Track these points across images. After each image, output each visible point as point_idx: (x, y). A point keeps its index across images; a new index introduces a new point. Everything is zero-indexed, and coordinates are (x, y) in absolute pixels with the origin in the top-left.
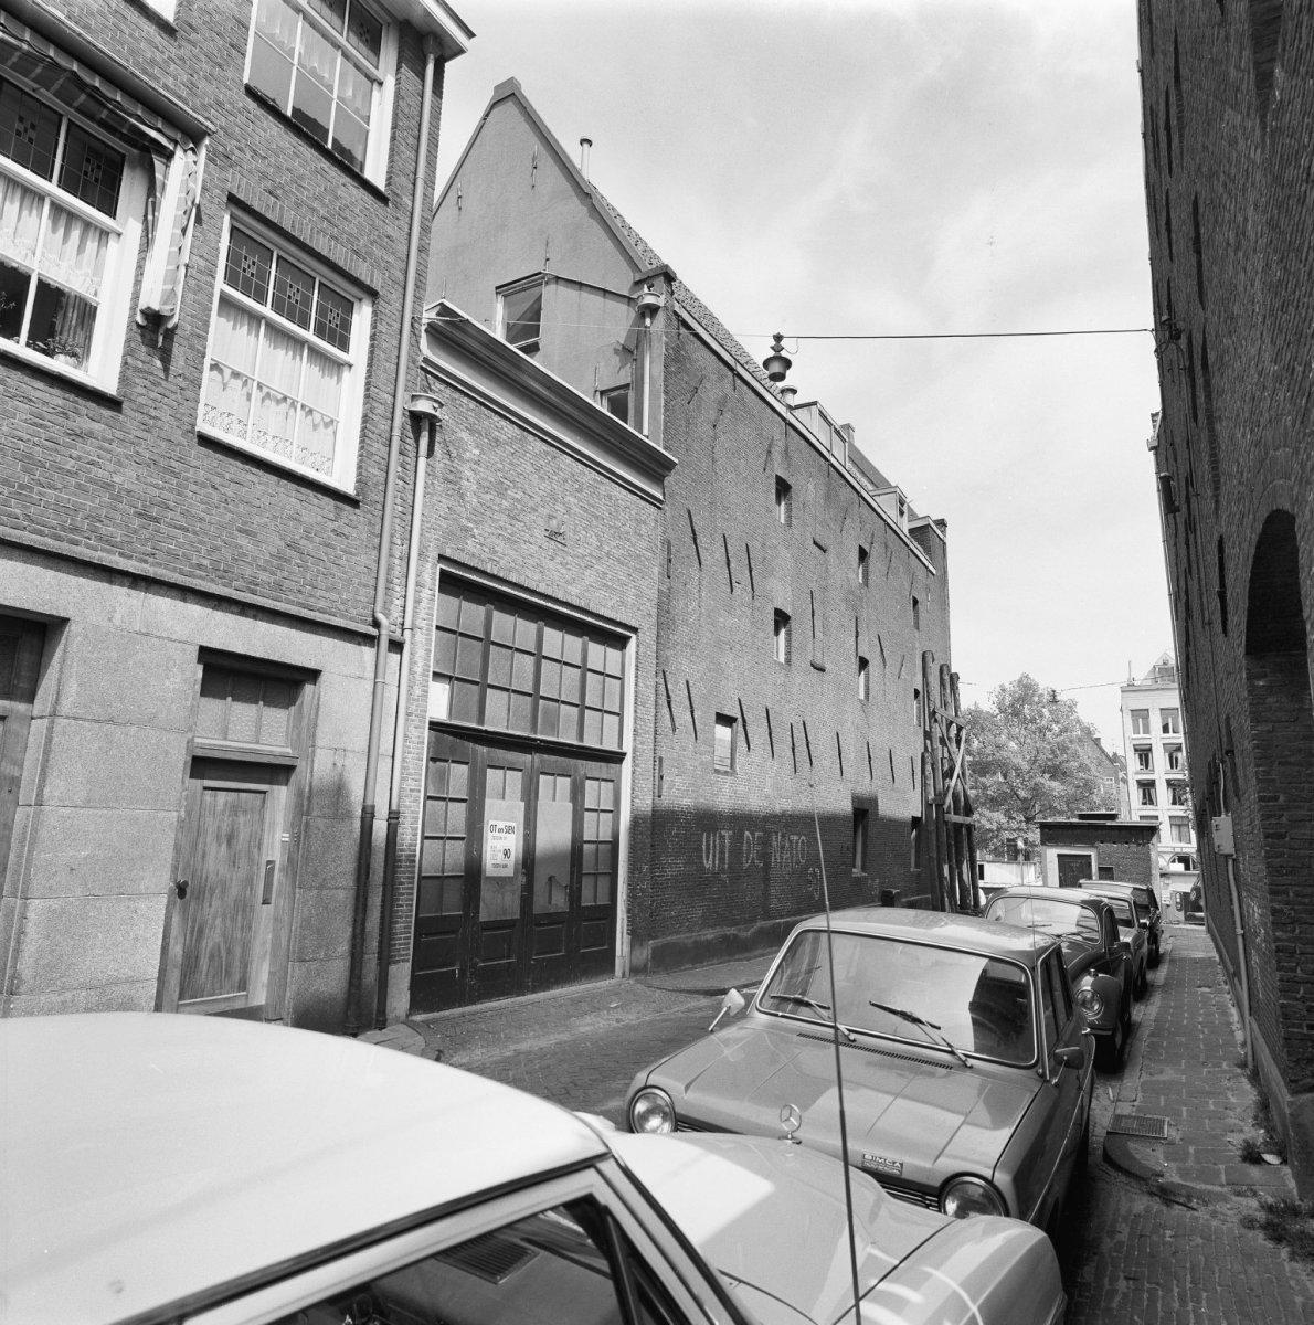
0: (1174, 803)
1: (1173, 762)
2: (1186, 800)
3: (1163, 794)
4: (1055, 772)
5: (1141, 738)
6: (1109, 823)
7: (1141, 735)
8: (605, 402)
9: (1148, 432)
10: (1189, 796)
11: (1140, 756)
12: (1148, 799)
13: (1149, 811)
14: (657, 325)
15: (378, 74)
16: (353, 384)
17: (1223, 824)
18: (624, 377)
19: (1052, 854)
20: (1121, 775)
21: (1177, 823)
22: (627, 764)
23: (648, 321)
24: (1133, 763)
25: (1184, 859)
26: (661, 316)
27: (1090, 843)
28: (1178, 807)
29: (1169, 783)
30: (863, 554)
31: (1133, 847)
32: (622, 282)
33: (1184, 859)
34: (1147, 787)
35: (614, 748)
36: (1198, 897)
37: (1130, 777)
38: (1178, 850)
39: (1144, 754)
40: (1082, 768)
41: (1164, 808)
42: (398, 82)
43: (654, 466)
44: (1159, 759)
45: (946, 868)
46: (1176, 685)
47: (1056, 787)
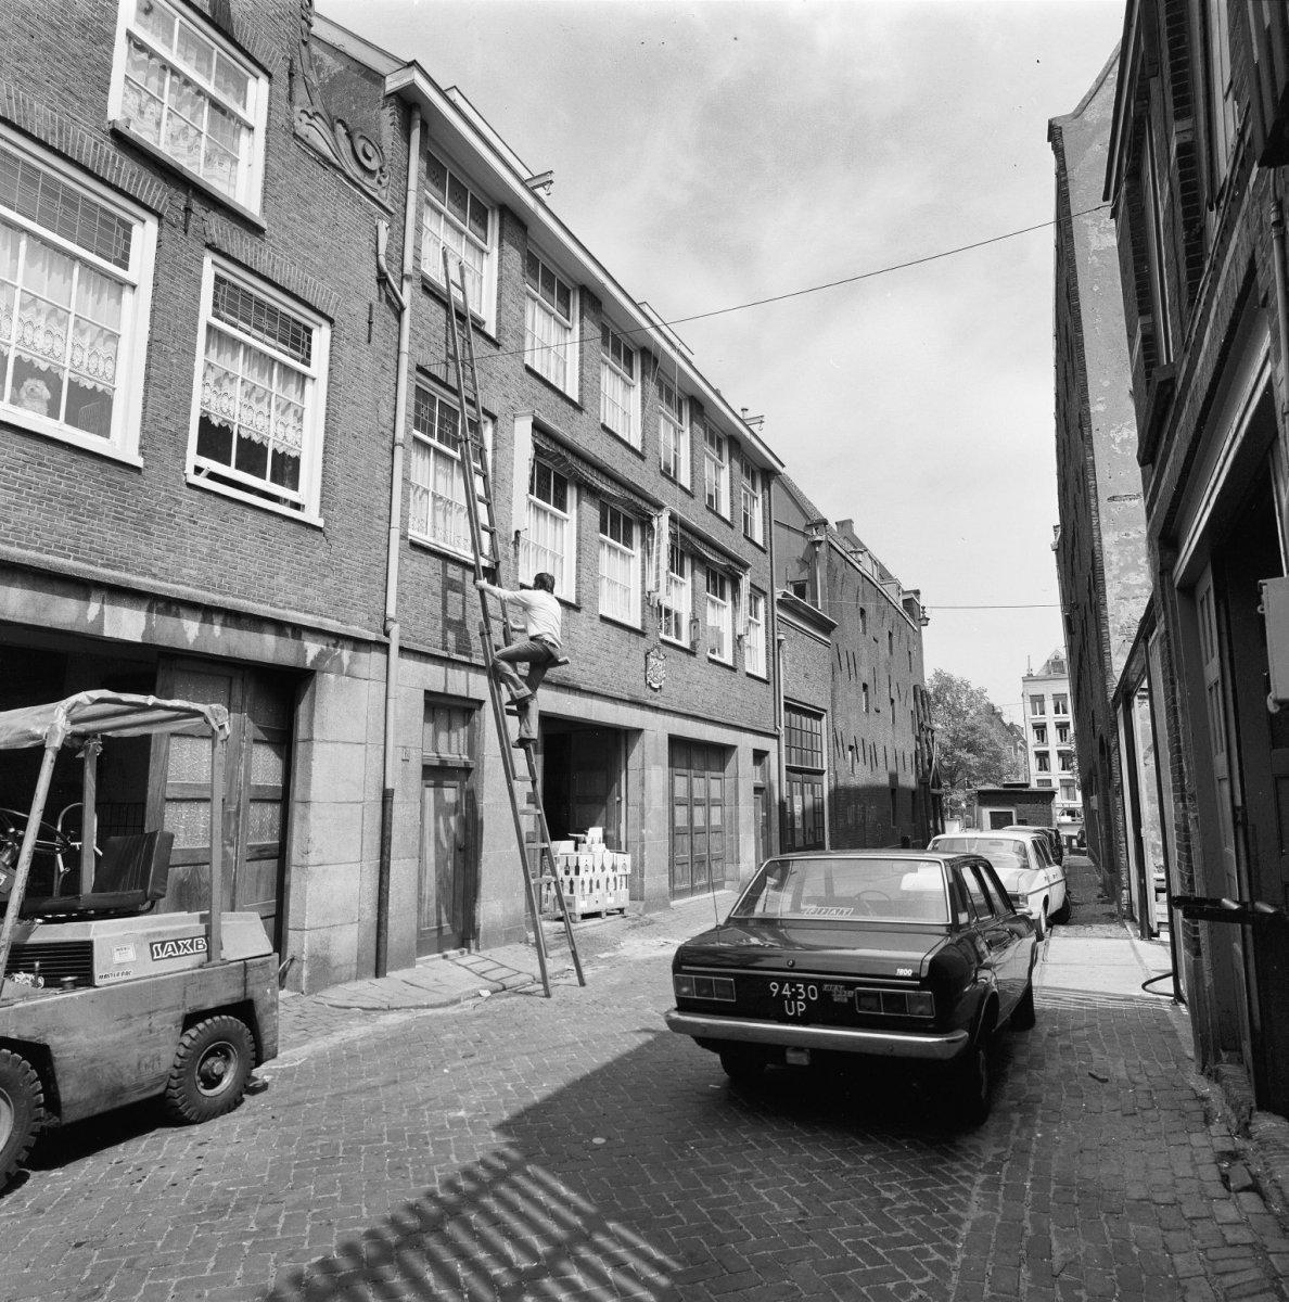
0: (1063, 769)
1: (1063, 736)
2: (1073, 767)
3: (1055, 762)
4: (971, 747)
5: (1039, 719)
6: (1024, 790)
7: (1039, 716)
8: (792, 587)
9: (1051, 538)
10: (1075, 764)
11: (1037, 732)
12: (1044, 766)
13: (1044, 775)
14: (820, 550)
15: (633, 382)
16: (315, 398)
17: (1094, 798)
18: (804, 576)
19: (986, 812)
20: (1019, 744)
21: (1066, 784)
22: (826, 775)
23: (817, 549)
24: (1031, 737)
25: (1071, 813)
26: (823, 545)
27: (1012, 805)
28: (1066, 772)
29: (1060, 754)
30: (890, 634)
31: (1041, 806)
32: (800, 524)
33: (1071, 813)
34: (1043, 757)
35: (820, 768)
36: (1083, 837)
37: (1029, 747)
38: (1066, 806)
39: (1040, 730)
40: (991, 743)
41: (1056, 773)
42: (582, 328)
43: (826, 627)
44: (1052, 734)
45: (931, 822)
46: (1066, 676)
47: (972, 760)
